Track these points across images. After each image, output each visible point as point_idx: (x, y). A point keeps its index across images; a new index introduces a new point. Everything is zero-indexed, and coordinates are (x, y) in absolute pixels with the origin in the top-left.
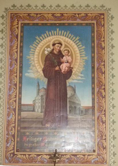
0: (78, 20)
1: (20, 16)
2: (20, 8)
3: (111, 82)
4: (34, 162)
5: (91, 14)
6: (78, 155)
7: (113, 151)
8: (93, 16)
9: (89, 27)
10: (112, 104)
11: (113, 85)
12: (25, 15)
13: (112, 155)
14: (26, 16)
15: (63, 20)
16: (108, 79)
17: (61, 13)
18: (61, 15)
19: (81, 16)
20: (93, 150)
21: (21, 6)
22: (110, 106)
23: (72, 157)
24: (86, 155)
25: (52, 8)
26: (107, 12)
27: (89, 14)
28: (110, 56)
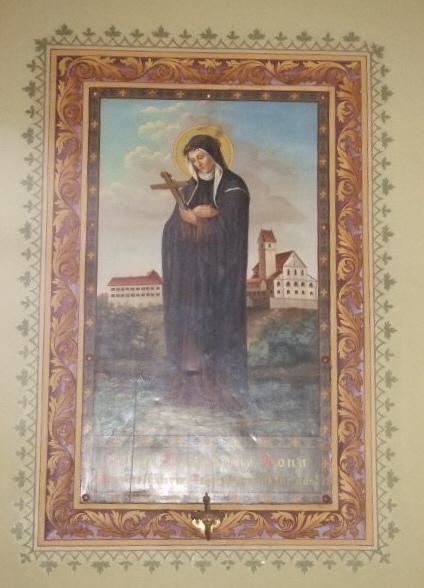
0: (274, 81)
1: (166, 66)
2: (131, 39)
3: (383, 399)
4: (142, 533)
5: (316, 62)
6: (276, 512)
7: (389, 520)
8: (319, 71)
9: (331, 95)
10: (385, 420)
11: (384, 121)
12: (103, 62)
13: (383, 334)
14: (109, 66)
15: (226, 81)
16: (373, 389)
17: (216, 56)
18: (218, 64)
19: (285, 68)
20: (324, 497)
21: (137, 34)
22: (380, 479)
23: (256, 516)
24: (338, 330)
25: (284, 43)
26: (369, 58)
27: (306, 61)
28: (383, 462)
